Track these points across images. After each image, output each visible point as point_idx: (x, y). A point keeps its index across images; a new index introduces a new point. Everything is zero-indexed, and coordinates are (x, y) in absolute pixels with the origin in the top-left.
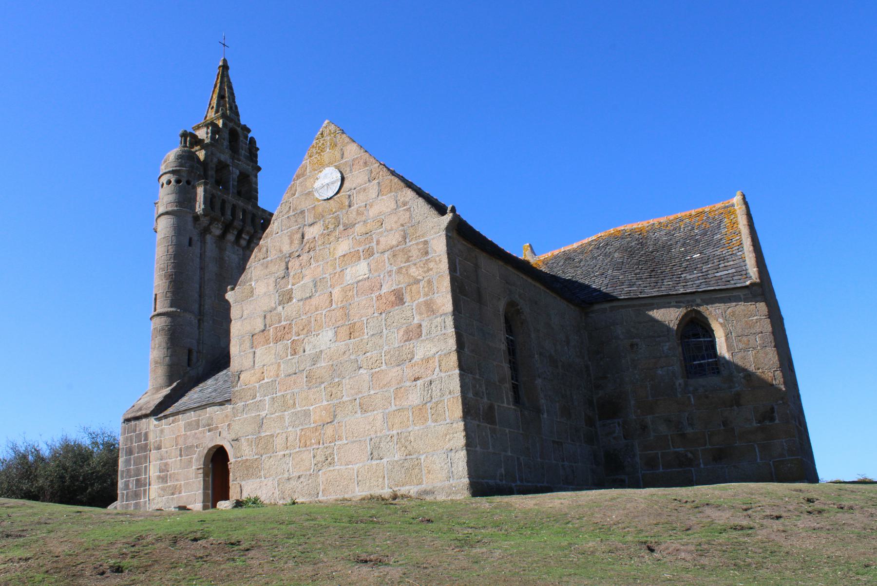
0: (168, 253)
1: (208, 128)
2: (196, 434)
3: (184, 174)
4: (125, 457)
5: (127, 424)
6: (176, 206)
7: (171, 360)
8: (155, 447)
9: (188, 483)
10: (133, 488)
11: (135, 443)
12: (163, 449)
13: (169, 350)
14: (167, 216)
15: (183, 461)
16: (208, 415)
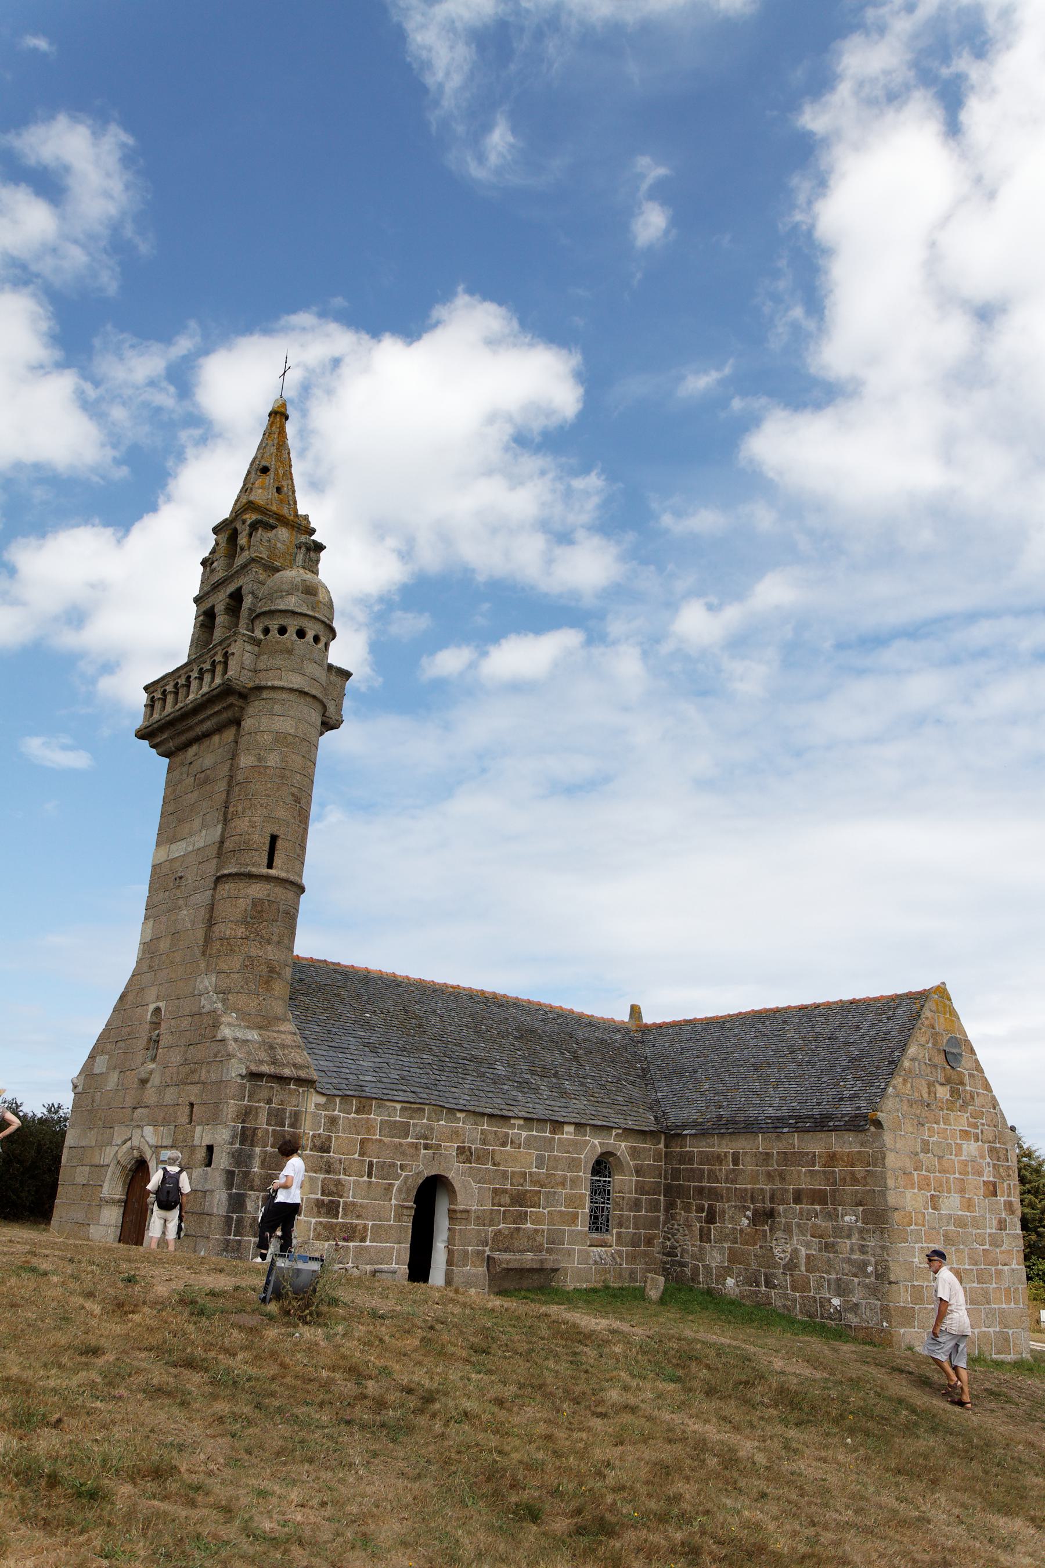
4: (238, 1146)
8: (315, 1146)
12: (331, 1154)
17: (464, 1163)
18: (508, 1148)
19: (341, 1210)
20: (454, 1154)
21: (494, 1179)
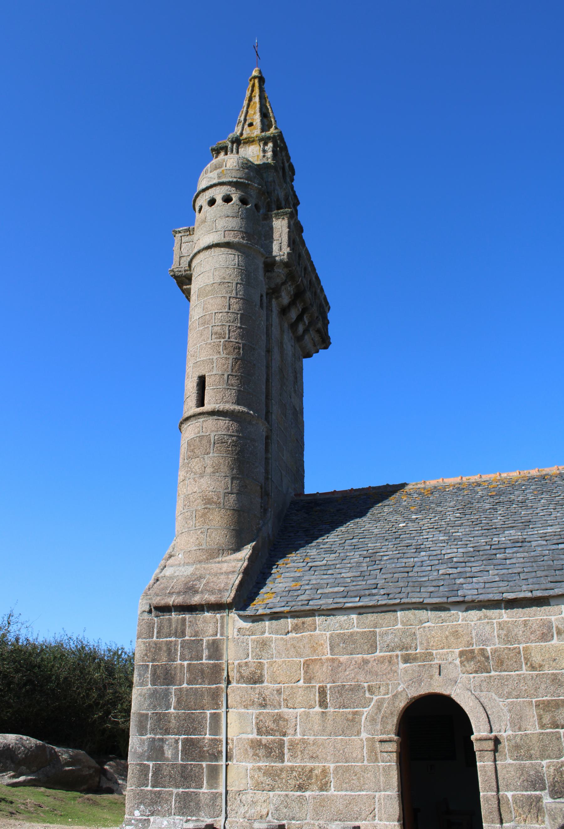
0: (229, 309)
1: (266, 144)
2: (366, 662)
3: (253, 193)
4: (150, 686)
5: (157, 616)
6: (243, 238)
7: (238, 500)
8: (242, 677)
9: (347, 769)
10: (176, 758)
11: (183, 658)
12: (265, 684)
13: (235, 482)
14: (227, 250)
15: (330, 718)
16: (400, 626)
17: (476, 672)
18: (555, 641)
19: (286, 751)
20: (458, 662)
21: (536, 689)
